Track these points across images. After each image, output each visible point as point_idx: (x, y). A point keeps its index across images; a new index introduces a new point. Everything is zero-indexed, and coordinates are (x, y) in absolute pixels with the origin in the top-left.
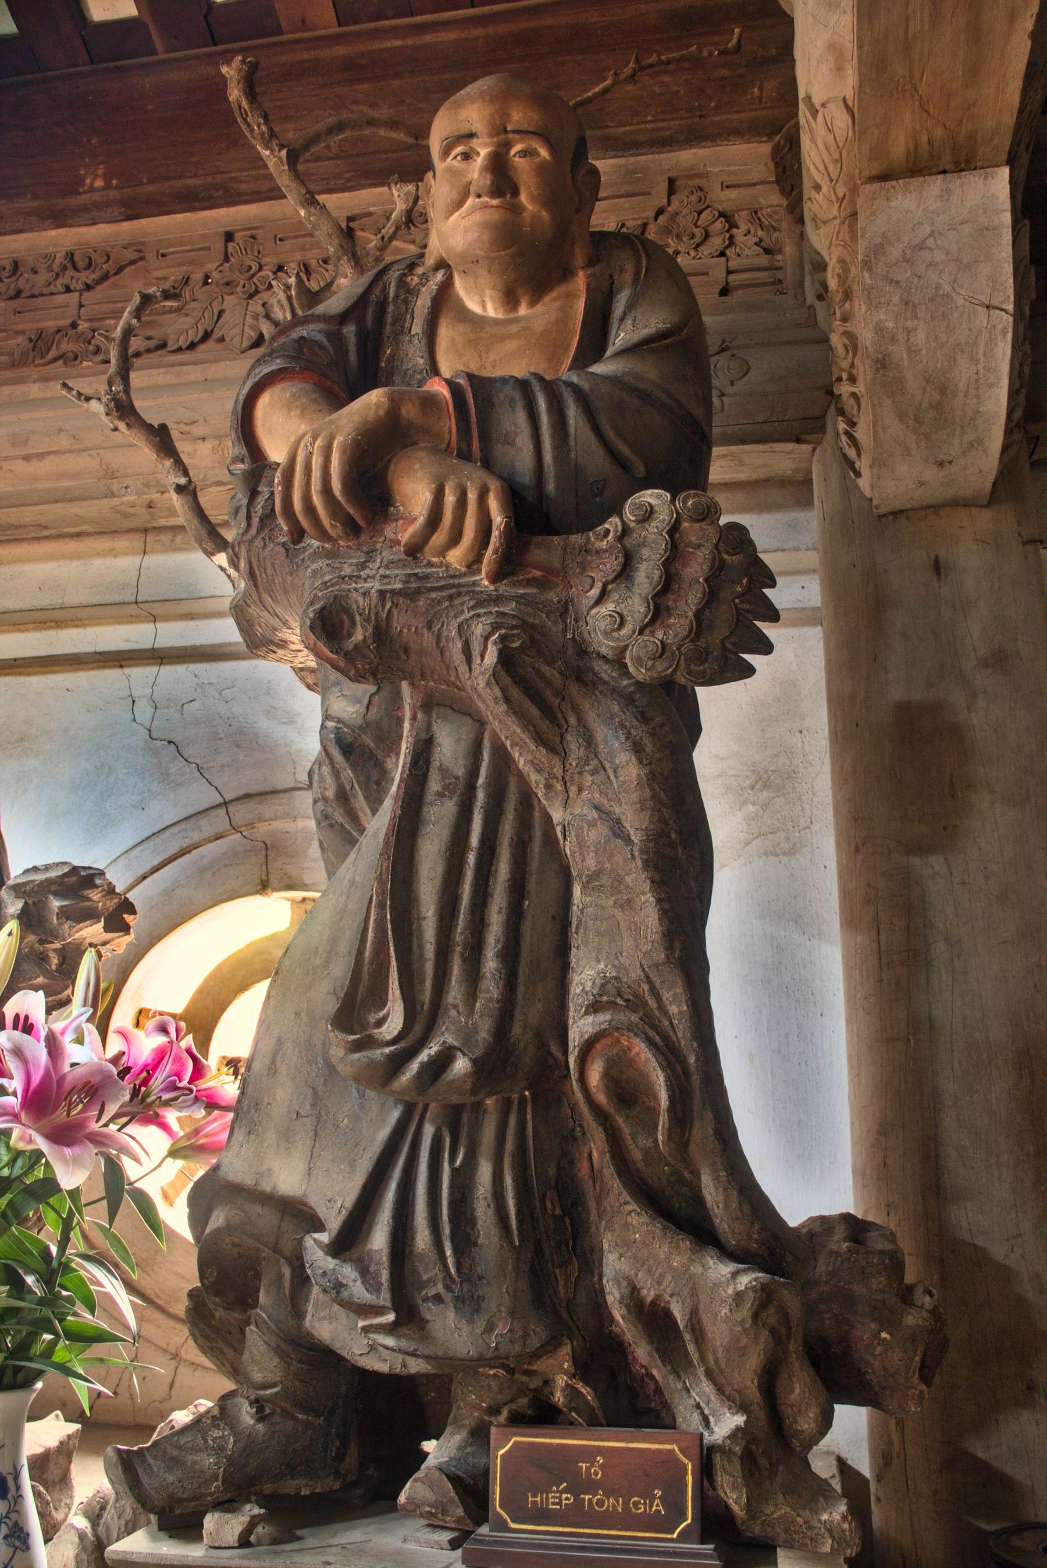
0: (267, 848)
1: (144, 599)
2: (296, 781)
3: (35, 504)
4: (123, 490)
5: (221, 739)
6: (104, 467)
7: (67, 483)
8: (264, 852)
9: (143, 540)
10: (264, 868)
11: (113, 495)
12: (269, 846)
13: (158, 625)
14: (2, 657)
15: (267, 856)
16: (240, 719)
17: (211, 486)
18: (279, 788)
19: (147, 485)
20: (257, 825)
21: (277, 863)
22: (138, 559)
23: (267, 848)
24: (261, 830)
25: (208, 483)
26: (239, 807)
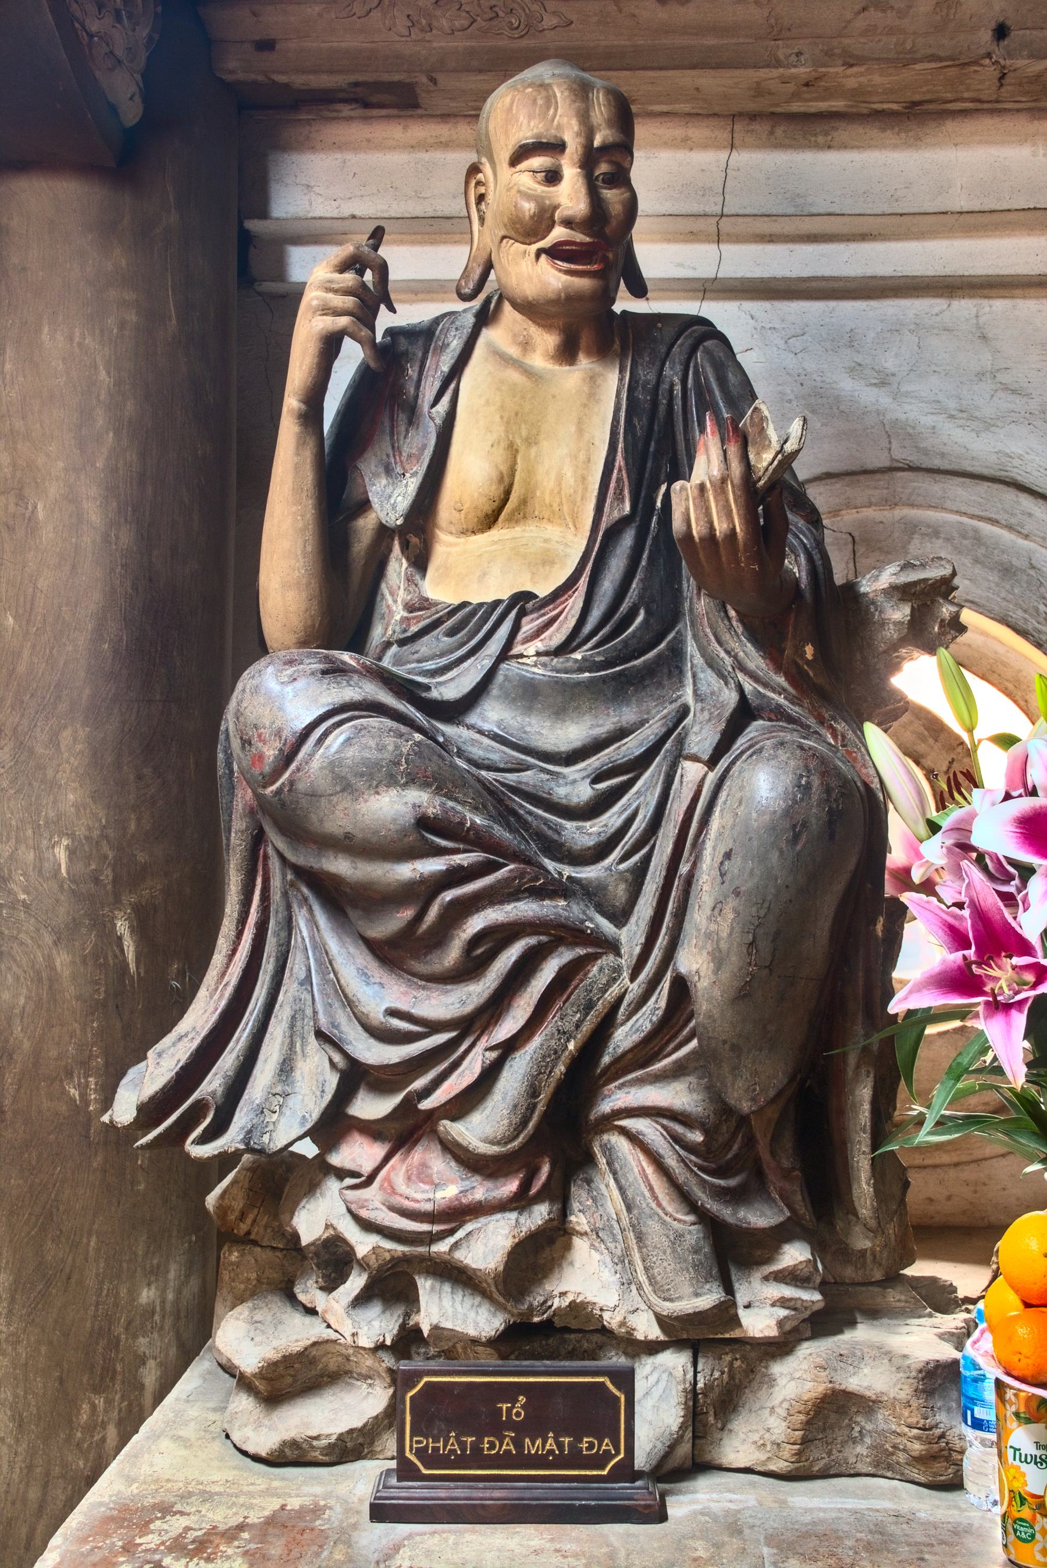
0: (854, 542)
1: (733, 212)
2: (892, 460)
3: (661, 69)
4: (793, 58)
5: (790, 401)
6: (772, 21)
7: (710, 41)
8: (850, 546)
9: (729, 129)
10: (851, 565)
11: (778, 64)
12: (857, 539)
13: (724, 247)
14: (1044, 301)
15: (854, 551)
16: (815, 376)
17: (921, 60)
18: (870, 466)
19: (829, 53)
20: (843, 512)
21: (869, 561)
22: (723, 155)
23: (854, 542)
24: (846, 518)
25: (918, 56)
26: (822, 489)
